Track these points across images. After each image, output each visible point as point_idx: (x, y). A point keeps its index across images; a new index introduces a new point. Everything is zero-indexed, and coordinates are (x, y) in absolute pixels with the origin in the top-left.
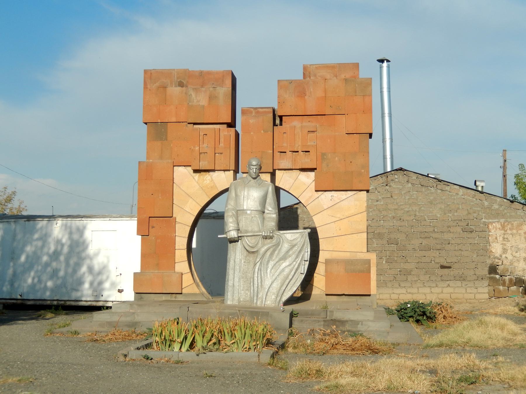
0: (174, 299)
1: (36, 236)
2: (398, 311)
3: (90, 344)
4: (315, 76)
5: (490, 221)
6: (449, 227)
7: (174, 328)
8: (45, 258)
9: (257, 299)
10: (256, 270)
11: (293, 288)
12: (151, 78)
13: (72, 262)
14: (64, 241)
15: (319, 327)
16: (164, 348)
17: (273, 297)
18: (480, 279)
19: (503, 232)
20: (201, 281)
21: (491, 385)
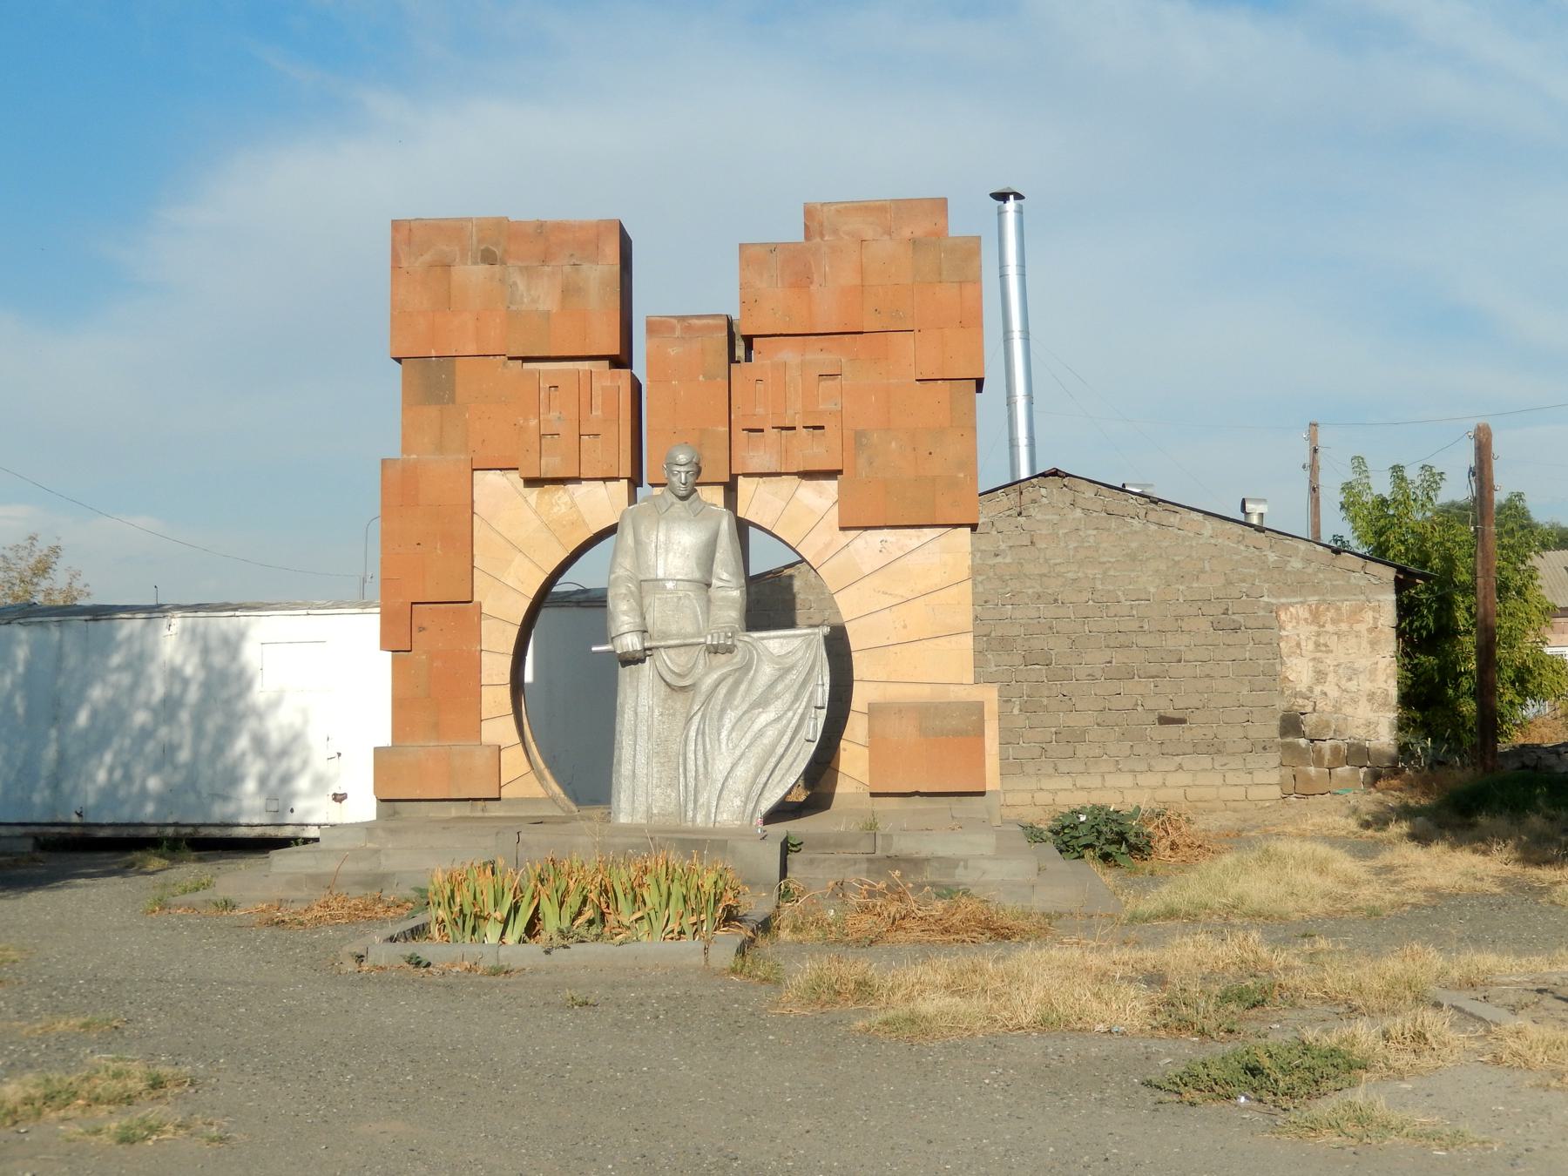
0: (480, 814)
1: (116, 659)
2: (1056, 833)
3: (267, 932)
4: (835, 232)
5: (1283, 600)
6: (1178, 618)
7: (486, 885)
8: (141, 717)
9: (695, 808)
10: (692, 734)
11: (785, 782)
12: (409, 242)
13: (211, 725)
14: (189, 670)
15: (856, 876)
16: (459, 937)
17: (738, 802)
18: (1259, 748)
19: (1315, 628)
20: (549, 766)
21: (1302, 1008)
